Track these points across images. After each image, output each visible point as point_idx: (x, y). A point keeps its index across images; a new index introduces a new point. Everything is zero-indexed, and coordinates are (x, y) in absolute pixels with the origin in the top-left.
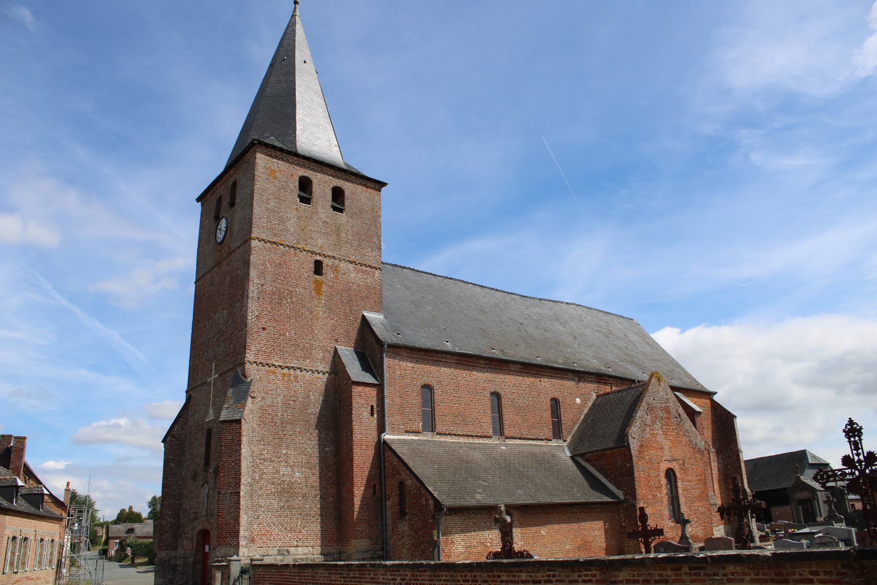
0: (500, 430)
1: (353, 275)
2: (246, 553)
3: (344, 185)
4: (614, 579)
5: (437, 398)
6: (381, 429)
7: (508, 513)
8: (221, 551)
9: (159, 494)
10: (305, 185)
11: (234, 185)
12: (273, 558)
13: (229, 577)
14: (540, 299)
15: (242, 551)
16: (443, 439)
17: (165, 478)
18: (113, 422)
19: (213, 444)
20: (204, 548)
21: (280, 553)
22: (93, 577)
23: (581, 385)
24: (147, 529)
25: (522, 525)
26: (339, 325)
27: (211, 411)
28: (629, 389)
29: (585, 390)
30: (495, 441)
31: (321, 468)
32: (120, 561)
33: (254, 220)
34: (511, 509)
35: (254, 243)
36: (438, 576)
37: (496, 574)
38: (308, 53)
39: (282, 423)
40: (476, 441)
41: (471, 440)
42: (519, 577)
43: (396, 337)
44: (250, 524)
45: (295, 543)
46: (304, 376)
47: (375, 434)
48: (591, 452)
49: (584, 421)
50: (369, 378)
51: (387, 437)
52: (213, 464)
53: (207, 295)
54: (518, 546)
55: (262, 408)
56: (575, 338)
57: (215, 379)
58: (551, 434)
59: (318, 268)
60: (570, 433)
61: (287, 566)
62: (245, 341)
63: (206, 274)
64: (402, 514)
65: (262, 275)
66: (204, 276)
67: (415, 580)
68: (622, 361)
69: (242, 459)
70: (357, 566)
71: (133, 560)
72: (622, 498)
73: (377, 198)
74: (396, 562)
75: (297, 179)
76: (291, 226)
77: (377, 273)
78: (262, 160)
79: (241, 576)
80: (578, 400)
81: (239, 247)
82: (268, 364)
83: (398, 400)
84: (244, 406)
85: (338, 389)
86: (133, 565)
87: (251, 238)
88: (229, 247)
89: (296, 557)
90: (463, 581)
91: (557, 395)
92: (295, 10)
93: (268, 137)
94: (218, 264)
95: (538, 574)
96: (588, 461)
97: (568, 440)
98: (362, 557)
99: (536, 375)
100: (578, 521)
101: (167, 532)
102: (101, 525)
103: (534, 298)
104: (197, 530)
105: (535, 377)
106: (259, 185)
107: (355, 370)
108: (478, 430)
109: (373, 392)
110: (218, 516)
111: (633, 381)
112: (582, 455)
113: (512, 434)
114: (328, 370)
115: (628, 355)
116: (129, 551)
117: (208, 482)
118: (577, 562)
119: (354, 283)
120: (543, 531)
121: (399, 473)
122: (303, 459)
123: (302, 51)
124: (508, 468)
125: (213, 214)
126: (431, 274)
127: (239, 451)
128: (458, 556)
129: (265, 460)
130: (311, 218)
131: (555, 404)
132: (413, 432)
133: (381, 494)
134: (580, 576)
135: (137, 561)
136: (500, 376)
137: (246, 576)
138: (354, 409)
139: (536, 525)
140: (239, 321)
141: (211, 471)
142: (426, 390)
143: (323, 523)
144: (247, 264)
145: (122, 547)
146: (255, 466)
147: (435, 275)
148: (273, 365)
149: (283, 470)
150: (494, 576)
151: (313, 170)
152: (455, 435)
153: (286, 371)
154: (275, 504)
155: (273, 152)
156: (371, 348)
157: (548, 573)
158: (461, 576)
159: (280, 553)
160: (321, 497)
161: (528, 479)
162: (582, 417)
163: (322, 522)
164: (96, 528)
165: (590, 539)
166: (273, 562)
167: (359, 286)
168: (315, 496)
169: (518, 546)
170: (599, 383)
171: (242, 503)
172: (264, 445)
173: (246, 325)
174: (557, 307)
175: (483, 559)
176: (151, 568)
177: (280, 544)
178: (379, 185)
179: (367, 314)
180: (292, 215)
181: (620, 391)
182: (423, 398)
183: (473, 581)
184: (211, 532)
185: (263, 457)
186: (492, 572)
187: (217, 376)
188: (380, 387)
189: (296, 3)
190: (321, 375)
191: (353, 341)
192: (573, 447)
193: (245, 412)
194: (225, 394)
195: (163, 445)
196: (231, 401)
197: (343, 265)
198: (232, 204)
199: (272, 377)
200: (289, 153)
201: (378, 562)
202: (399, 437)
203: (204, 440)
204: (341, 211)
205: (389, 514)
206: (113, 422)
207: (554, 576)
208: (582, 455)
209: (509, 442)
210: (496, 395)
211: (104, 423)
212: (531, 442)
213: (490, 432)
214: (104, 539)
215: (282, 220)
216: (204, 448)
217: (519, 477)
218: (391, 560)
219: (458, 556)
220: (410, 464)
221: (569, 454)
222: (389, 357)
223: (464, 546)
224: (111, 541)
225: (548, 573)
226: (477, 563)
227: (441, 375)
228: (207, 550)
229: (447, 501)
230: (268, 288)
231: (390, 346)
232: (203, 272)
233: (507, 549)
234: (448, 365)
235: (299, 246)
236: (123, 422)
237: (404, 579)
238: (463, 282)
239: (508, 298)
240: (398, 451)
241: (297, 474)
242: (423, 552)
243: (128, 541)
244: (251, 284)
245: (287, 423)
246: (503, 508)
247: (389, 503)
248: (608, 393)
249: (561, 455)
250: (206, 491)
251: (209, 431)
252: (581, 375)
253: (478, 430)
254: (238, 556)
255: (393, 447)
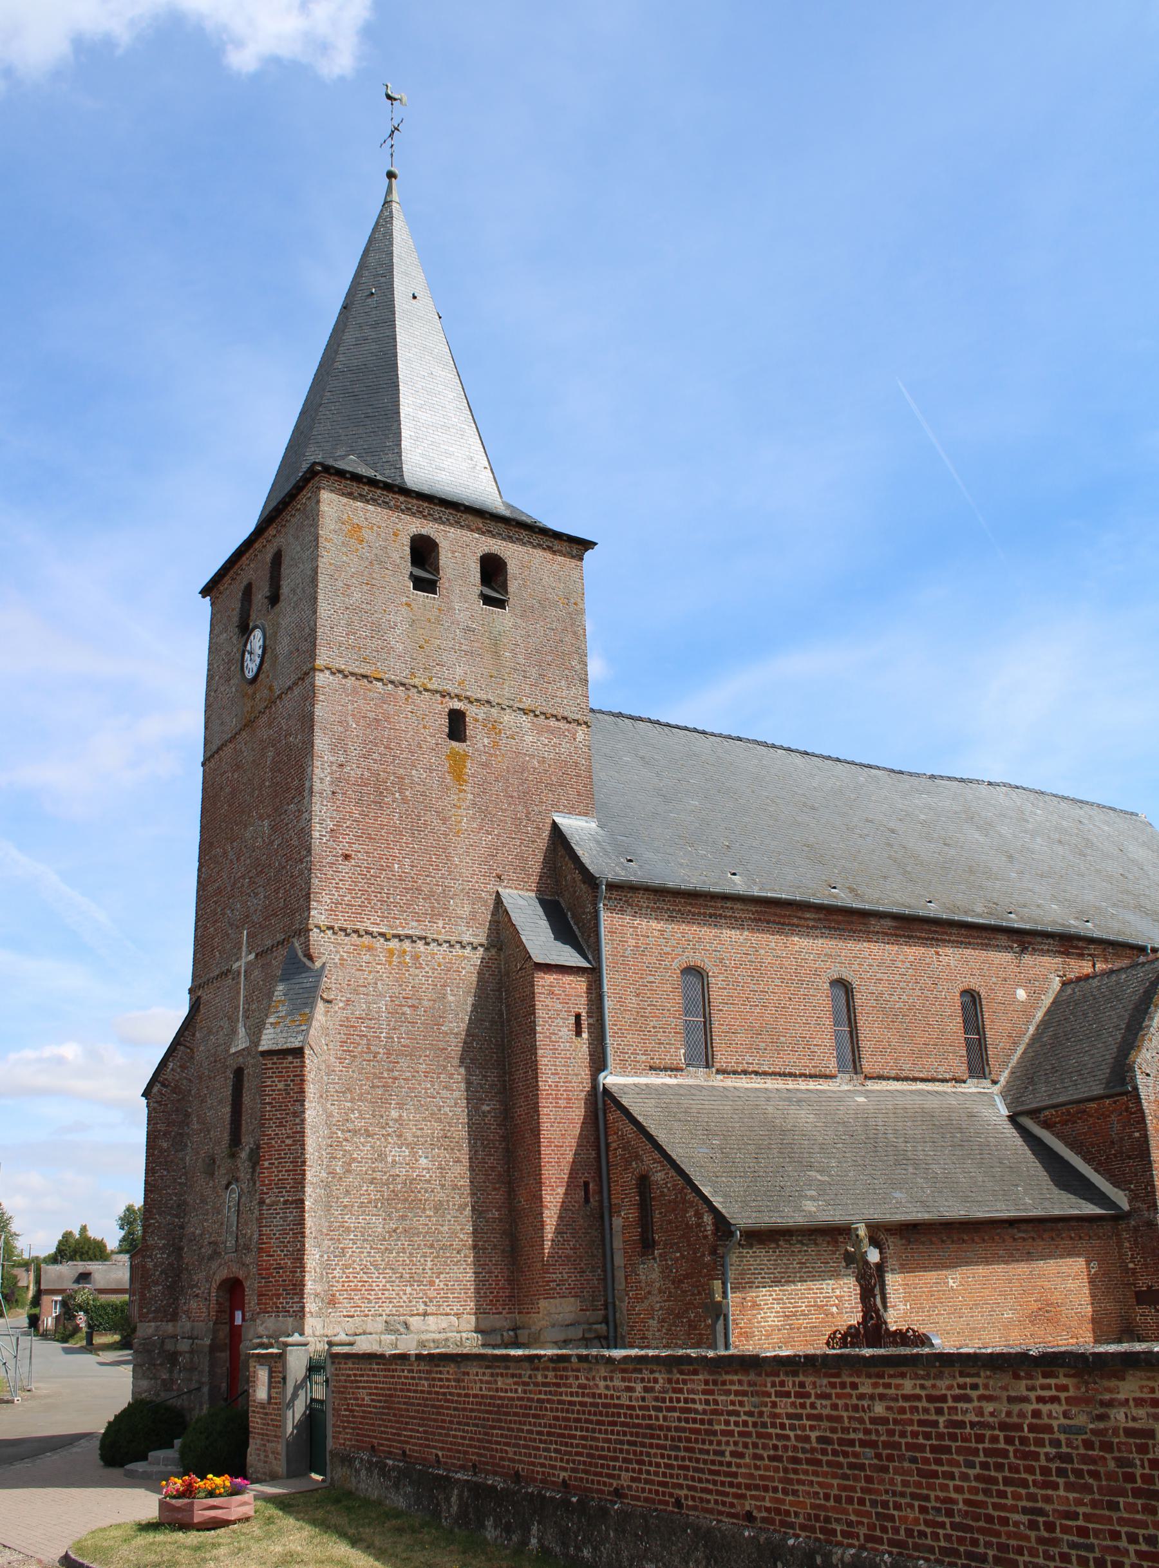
0: (853, 1060)
1: (530, 738)
2: (321, 1328)
3: (502, 551)
4: (1107, 1397)
5: (715, 995)
6: (598, 1062)
7: (875, 1242)
8: (266, 1325)
9: (138, 1201)
10: (423, 553)
11: (277, 559)
12: (374, 1340)
13: (284, 1378)
14: (932, 777)
15: (312, 1324)
16: (730, 1082)
17: (149, 1171)
18: (49, 1051)
19: (246, 1099)
20: (232, 1318)
21: (389, 1329)
22: (11, 1373)
23: (1027, 959)
24: (115, 1273)
25: (904, 1268)
26: (504, 845)
27: (242, 1031)
28: (1133, 966)
29: (1037, 970)
30: (842, 1085)
31: (472, 1147)
32: (64, 1340)
33: (320, 631)
34: (879, 1233)
35: (321, 679)
36: (724, 1383)
37: (848, 1380)
38: (421, 277)
39: (389, 1054)
40: (802, 1085)
41: (791, 1084)
42: (898, 1387)
43: (625, 868)
44: (327, 1267)
45: (422, 1307)
46: (433, 955)
47: (585, 1073)
48: (1054, 1106)
49: (1035, 1039)
50: (568, 956)
51: (610, 1079)
52: (248, 1141)
53: (228, 790)
54: (895, 1319)
55: (346, 1024)
56: (1010, 857)
57: (247, 963)
58: (964, 1067)
59: (457, 726)
60: (1005, 1064)
61: (404, 1357)
62: (308, 883)
63: (224, 745)
64: (646, 1245)
65: (339, 744)
66: (219, 749)
67: (675, 1391)
68: (1114, 905)
69: (308, 1131)
70: (552, 1359)
71: (90, 1338)
72: (1126, 1207)
73: (575, 575)
74: (633, 1352)
75: (407, 542)
76: (398, 640)
77: (581, 733)
78: (332, 505)
79: (308, 1377)
80: (1021, 994)
81: (290, 688)
82: (356, 931)
83: (632, 1002)
84: (309, 1020)
85: (505, 987)
86: (90, 1347)
87: (314, 669)
88: (271, 688)
89: (424, 1337)
90: (778, 1394)
91: (974, 983)
92: (389, 190)
93: (343, 457)
94: (249, 724)
95: (939, 1383)
96: (1047, 1125)
97: (1003, 1079)
98: (562, 1337)
99: (926, 941)
100: (1029, 1257)
101: (156, 1283)
102: (26, 1265)
103: (918, 775)
104: (218, 1278)
105: (925, 945)
106: (325, 561)
107: (538, 938)
108: (805, 1061)
109: (579, 985)
110: (260, 1250)
111: (1142, 949)
112: (1033, 1113)
113: (878, 1070)
114: (484, 942)
115: (1128, 892)
116: (81, 1319)
117: (237, 1180)
118: (1024, 1357)
119: (532, 756)
120: (953, 1279)
121: (638, 1158)
122: (433, 1128)
123: (407, 274)
124: (873, 1143)
125: (235, 619)
126: (695, 730)
127: (299, 1115)
128: (768, 1336)
129: (355, 1132)
130: (438, 621)
131: (972, 1000)
132: (665, 1069)
133: (601, 1202)
134: (1031, 1388)
135: (98, 1340)
136: (850, 944)
137: (319, 1378)
138: (540, 1021)
139: (936, 1268)
140: (295, 842)
141: (244, 1155)
142: (693, 979)
143: (480, 1264)
144: (307, 722)
145: (68, 1310)
146: (334, 1145)
147: (704, 733)
148: (367, 932)
149: (395, 1153)
150: (843, 1385)
151: (439, 520)
152: (756, 1073)
153: (394, 944)
154: (378, 1225)
155: (354, 487)
156: (572, 894)
157: (961, 1380)
158: (773, 1385)
159: (389, 1329)
160: (473, 1209)
161: (916, 1166)
162: (1032, 1030)
163: (477, 1262)
164: (16, 1271)
165: (1056, 1297)
166: (375, 1348)
167: (543, 761)
168: (462, 1208)
169: (895, 1319)
170: (1066, 953)
171: (309, 1222)
172: (352, 1101)
173: (309, 851)
174: (968, 791)
175: (818, 1347)
176: (126, 1354)
177: (389, 1308)
178: (579, 546)
179: (562, 821)
180: (399, 617)
181: (1112, 971)
182: (685, 996)
183: (799, 1395)
184: (247, 1284)
185: (350, 1126)
186: (838, 1375)
187: (252, 956)
188: (594, 974)
189: (391, 175)
190: (468, 951)
191: (535, 878)
192: (1013, 1095)
193: (312, 1031)
194: (270, 995)
195: (144, 1101)
196: (283, 1010)
197: (508, 718)
198: (274, 599)
199: (367, 958)
200: (388, 487)
201: (594, 1352)
202: (636, 1080)
203: (228, 1092)
204: (500, 604)
205: (618, 1243)
206: (49, 1051)
207: (975, 1387)
208: (1033, 1113)
209: (871, 1085)
210: (843, 987)
211: (30, 1054)
212: (920, 1086)
213: (832, 1066)
214: (31, 1294)
215: (377, 630)
216: (228, 1109)
217: (897, 1163)
218: (624, 1347)
219: (768, 1336)
220: (662, 1137)
221: (1004, 1112)
222: (612, 910)
223: (782, 1315)
224: (46, 1299)
225: (961, 1380)
226: (806, 1356)
227: (723, 945)
228: (238, 1321)
229: (741, 1216)
230: (353, 772)
231: (611, 886)
232: (214, 748)
233: (872, 1328)
234: (737, 923)
235: (416, 681)
236: (70, 1051)
237: (652, 1390)
238: (765, 744)
239: (863, 776)
240: (635, 1111)
241: (423, 1161)
242: (692, 1326)
243: (79, 1299)
244: (317, 763)
245: (400, 1054)
246: (862, 1232)
247: (618, 1222)
248: (1087, 977)
249: (986, 1112)
250: (236, 1196)
251: (239, 1073)
252: (1024, 939)
253: (805, 1061)
254: (302, 1334)
255: (625, 1102)
